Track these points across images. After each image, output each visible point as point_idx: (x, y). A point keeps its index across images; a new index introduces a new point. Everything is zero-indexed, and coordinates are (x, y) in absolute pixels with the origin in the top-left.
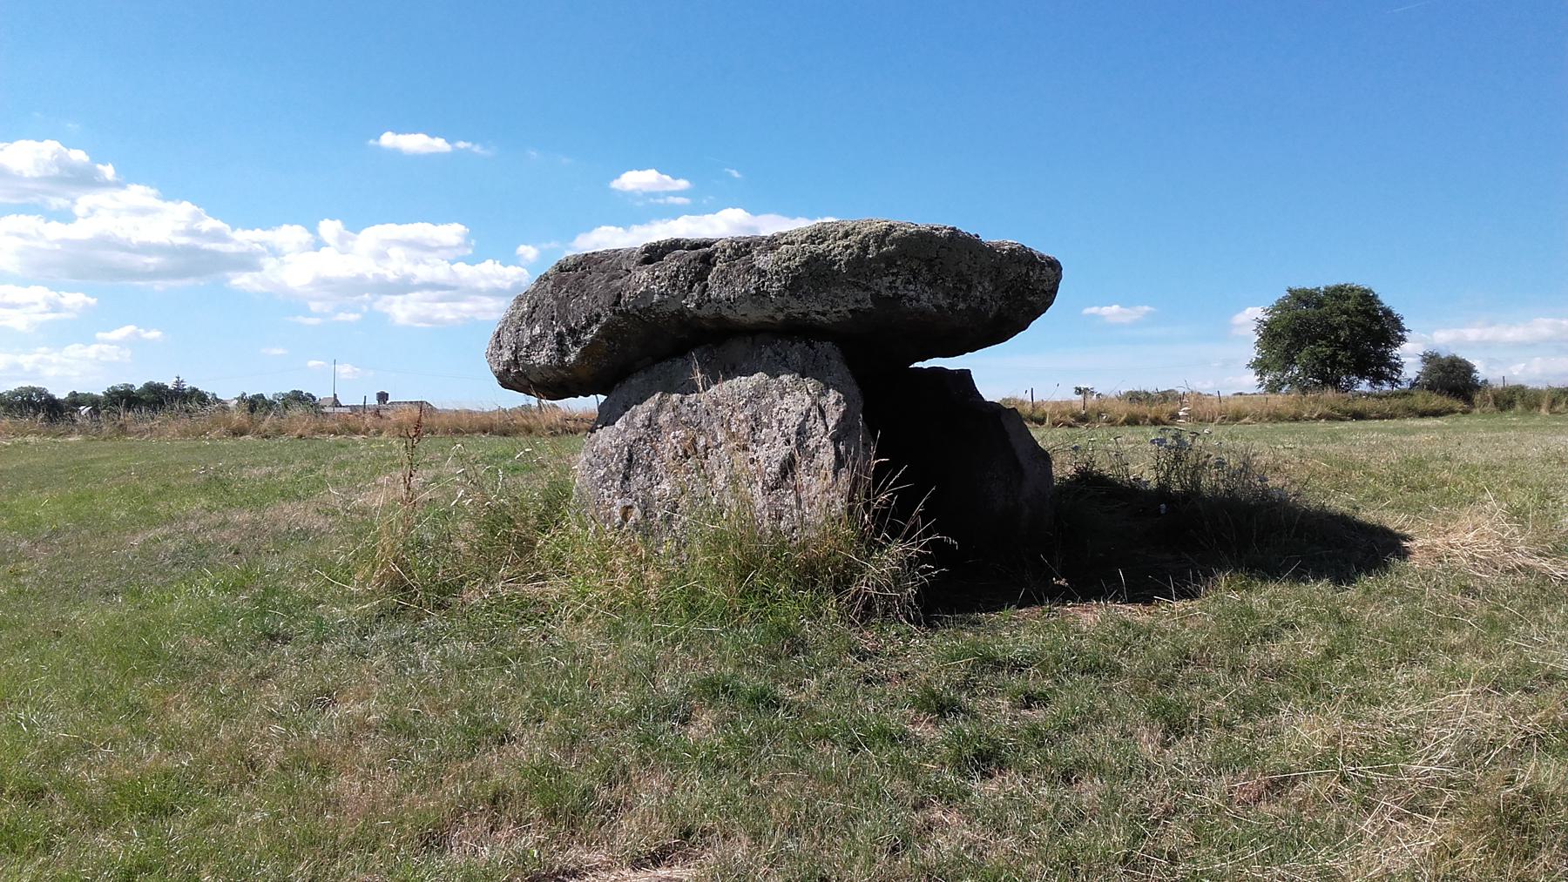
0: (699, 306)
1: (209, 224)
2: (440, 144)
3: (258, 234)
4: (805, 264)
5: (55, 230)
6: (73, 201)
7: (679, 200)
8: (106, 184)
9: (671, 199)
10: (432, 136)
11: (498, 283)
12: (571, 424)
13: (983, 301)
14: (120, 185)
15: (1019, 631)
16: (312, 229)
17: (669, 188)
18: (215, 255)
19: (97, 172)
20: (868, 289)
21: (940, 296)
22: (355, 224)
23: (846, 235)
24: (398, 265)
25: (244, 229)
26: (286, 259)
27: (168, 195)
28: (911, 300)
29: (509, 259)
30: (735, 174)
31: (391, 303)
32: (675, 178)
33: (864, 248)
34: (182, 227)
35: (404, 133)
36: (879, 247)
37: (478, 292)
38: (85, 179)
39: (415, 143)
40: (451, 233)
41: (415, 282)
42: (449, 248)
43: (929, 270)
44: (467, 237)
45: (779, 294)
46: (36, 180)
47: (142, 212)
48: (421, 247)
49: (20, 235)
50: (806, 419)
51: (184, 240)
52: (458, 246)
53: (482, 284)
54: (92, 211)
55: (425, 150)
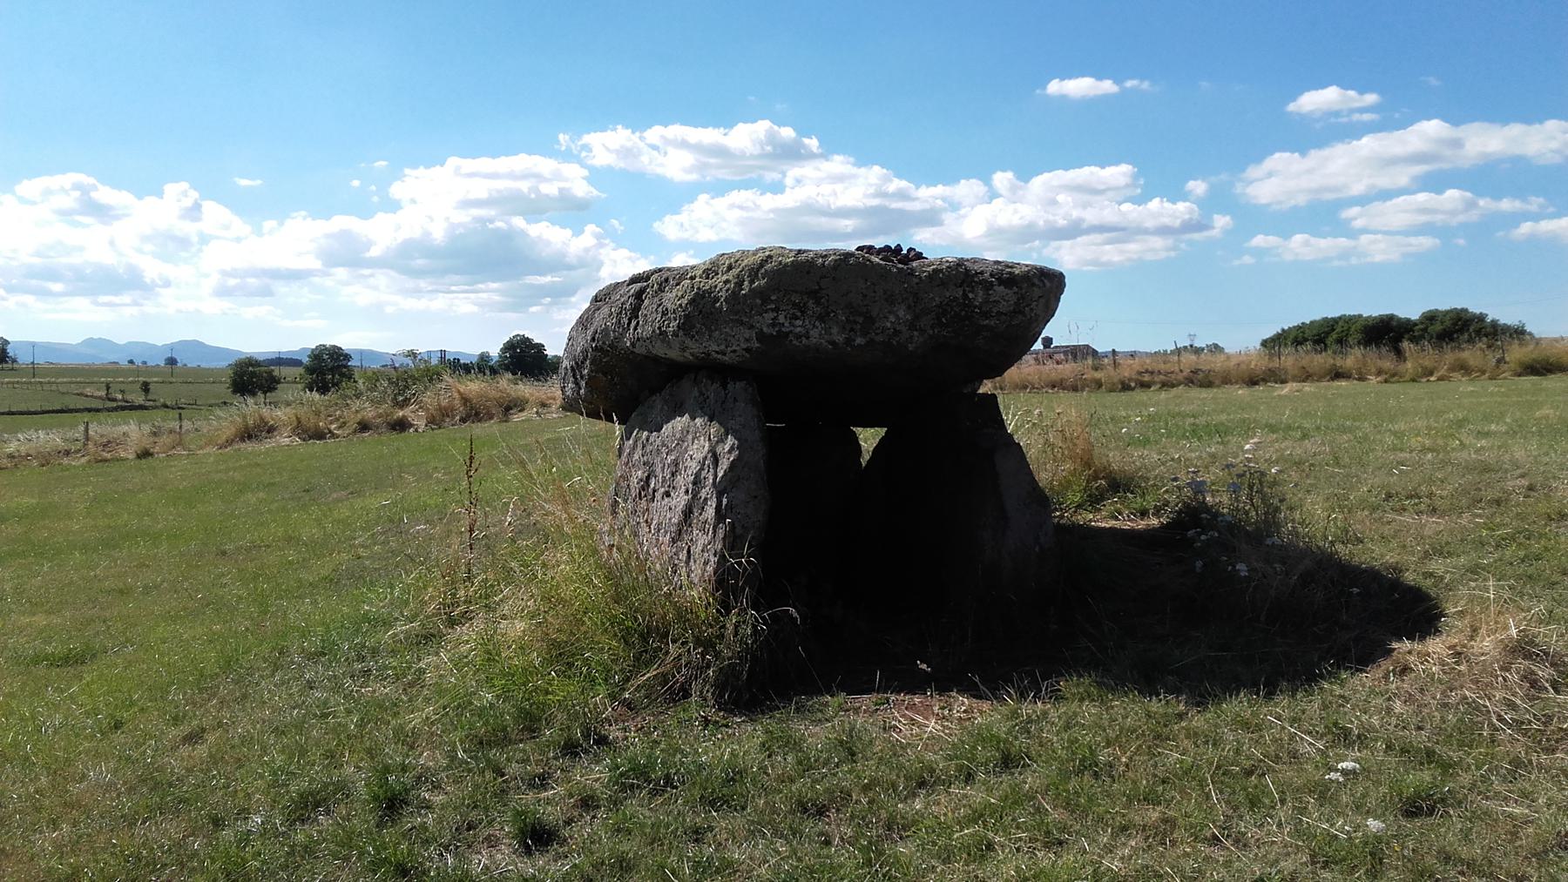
0: (633, 344)
1: (897, 184)
2: (1108, 86)
3: (939, 190)
4: (692, 302)
5: (769, 202)
6: (784, 175)
7: (1366, 117)
8: (811, 156)
9: (1356, 117)
10: (1099, 78)
11: (1166, 221)
12: (1147, 378)
13: (897, 332)
14: (825, 156)
15: (823, 725)
16: (987, 181)
17: (1357, 105)
18: (902, 213)
19: (804, 146)
20: (752, 327)
21: (835, 330)
22: (1025, 174)
23: (730, 268)
24: (1068, 209)
25: (928, 186)
26: (963, 212)
27: (863, 160)
28: (798, 337)
29: (1177, 195)
30: (1433, 81)
31: (1058, 249)
32: (1361, 93)
33: (740, 284)
34: (872, 190)
35: (1070, 78)
36: (752, 282)
37: (1146, 232)
38: (792, 153)
39: (1079, 86)
40: (1118, 174)
41: (1085, 226)
42: (1117, 189)
43: (818, 303)
44: (1135, 177)
45: (675, 334)
46: (752, 157)
47: (840, 178)
48: (1091, 191)
49: (741, 208)
50: (702, 469)
51: (876, 202)
52: (1127, 186)
53: (1150, 224)
54: (798, 181)
55: (1092, 93)
